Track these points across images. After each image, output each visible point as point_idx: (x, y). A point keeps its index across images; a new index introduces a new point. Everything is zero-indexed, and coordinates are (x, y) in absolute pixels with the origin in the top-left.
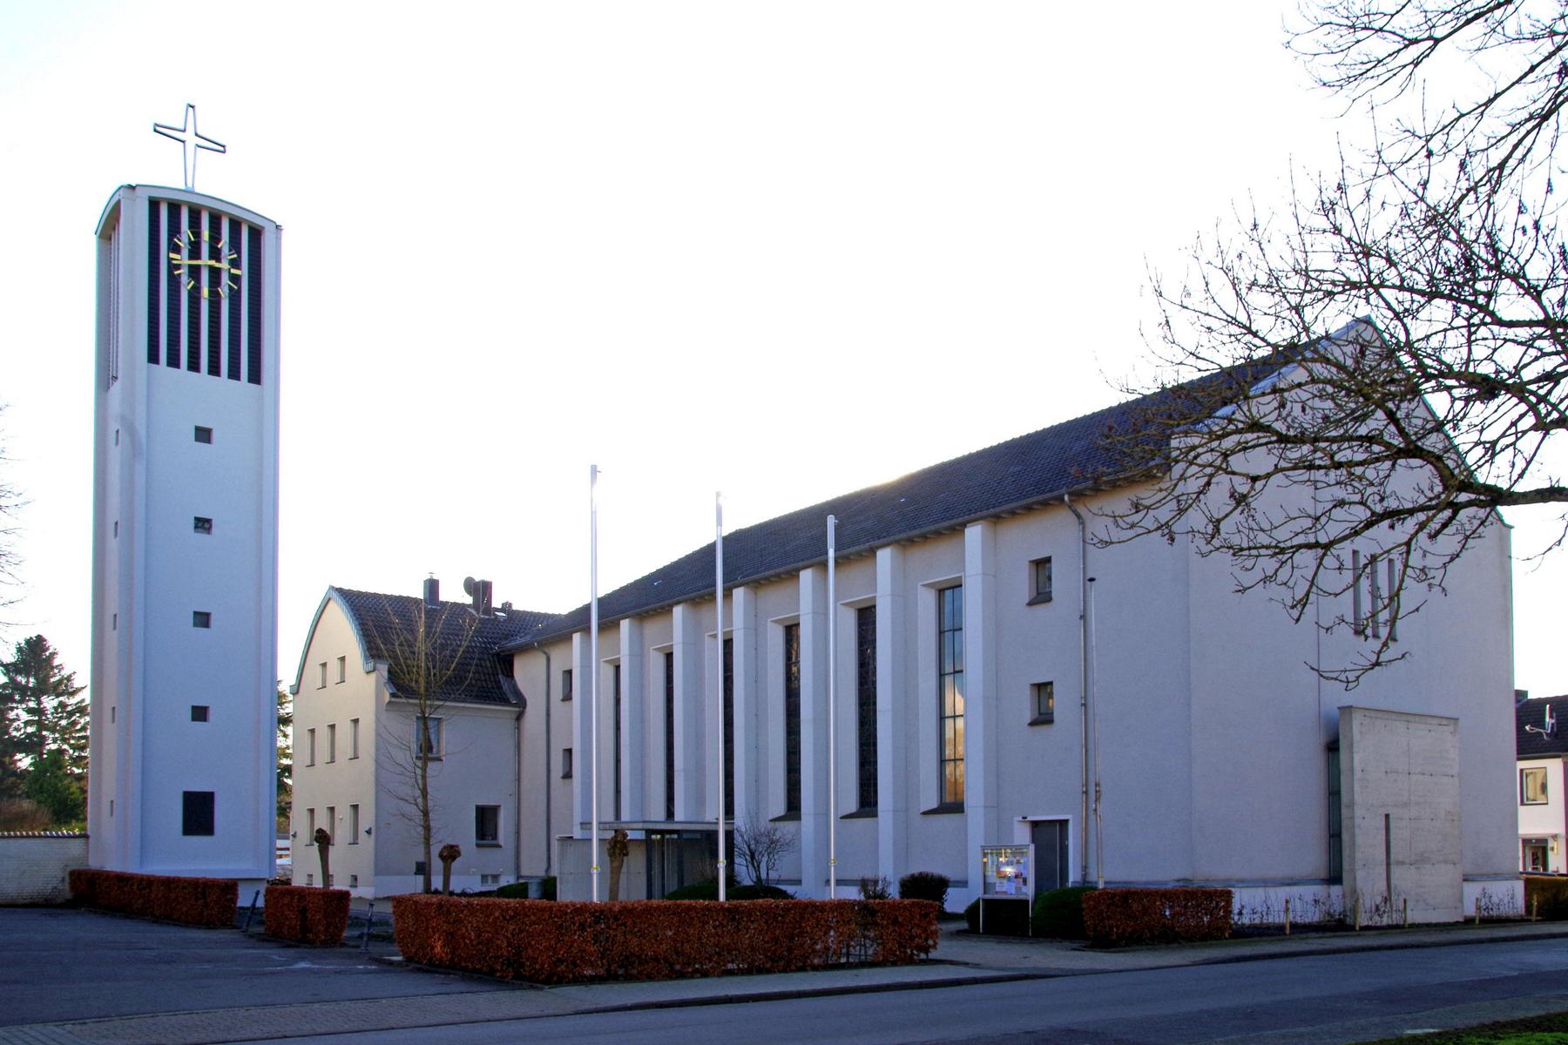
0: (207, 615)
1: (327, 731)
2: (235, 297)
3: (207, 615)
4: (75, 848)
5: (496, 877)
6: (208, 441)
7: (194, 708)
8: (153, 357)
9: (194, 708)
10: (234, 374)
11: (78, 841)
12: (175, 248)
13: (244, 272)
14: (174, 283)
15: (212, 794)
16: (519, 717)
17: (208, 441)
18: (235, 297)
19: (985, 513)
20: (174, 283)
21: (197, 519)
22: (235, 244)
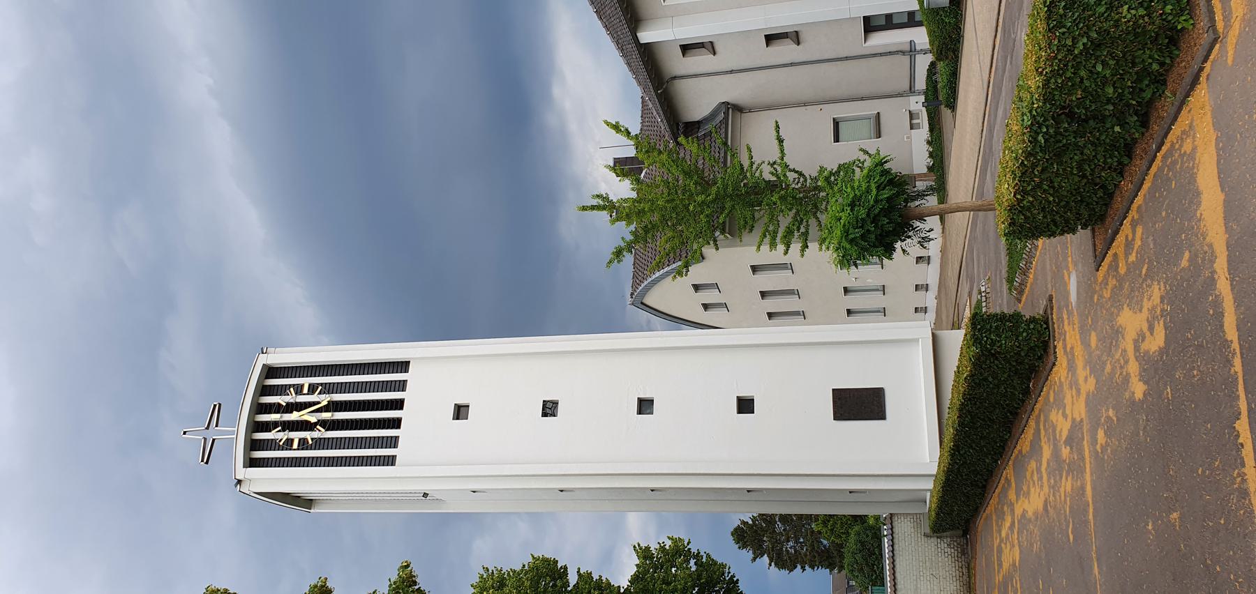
0: (641, 401)
1: (760, 276)
2: (328, 389)
3: (641, 401)
4: (904, 528)
5: (912, 115)
6: (555, 403)
7: (740, 412)
8: (390, 461)
9: (740, 412)
10: (401, 386)
11: (895, 524)
12: (289, 442)
13: (306, 381)
14: (320, 444)
15: (883, 418)
16: (738, 109)
17: (555, 403)
18: (328, 389)
19: (709, 127)
20: (320, 444)
21: (545, 415)
22: (281, 390)
